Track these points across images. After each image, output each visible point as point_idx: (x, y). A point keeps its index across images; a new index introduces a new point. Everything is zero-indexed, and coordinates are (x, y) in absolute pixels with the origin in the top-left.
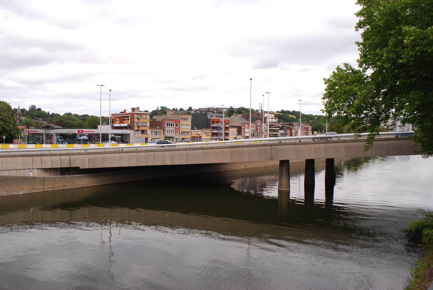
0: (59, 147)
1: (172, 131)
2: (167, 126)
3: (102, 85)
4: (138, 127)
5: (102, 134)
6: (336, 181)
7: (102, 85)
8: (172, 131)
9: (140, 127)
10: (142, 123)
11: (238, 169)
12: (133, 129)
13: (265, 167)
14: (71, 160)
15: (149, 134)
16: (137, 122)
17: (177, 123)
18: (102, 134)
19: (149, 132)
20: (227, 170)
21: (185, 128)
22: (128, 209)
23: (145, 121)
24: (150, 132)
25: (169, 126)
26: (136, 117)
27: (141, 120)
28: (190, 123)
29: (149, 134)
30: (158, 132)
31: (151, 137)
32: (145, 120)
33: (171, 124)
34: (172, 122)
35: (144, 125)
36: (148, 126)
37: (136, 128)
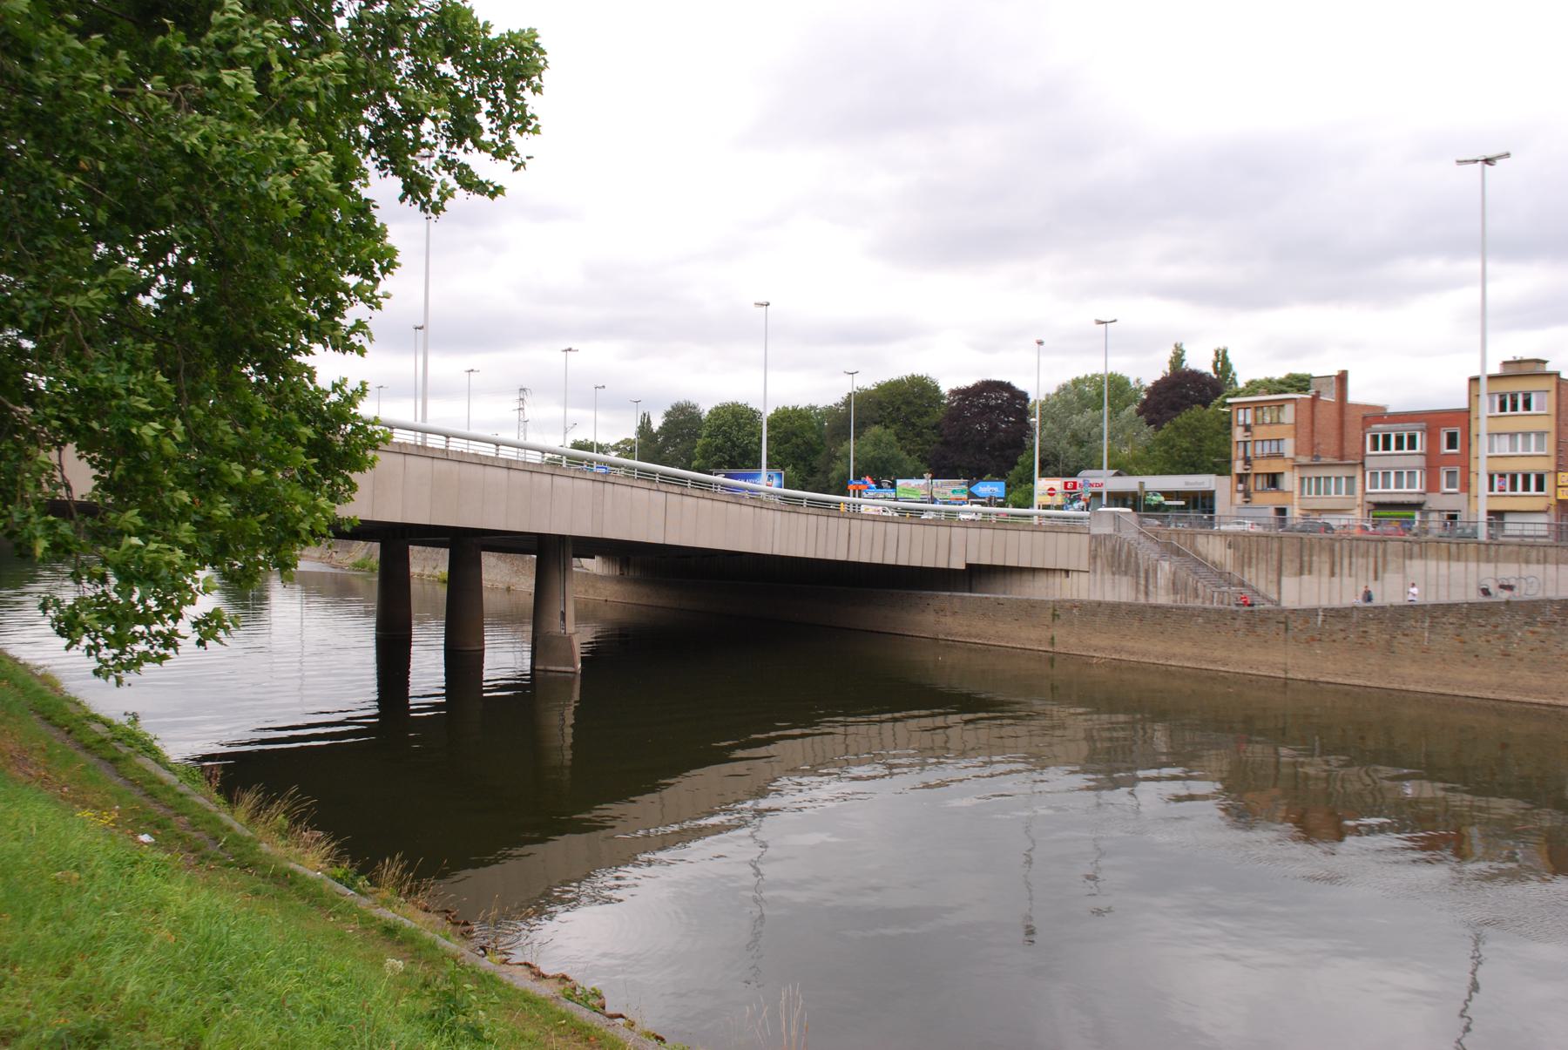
0: (1354, 560)
1: (1399, 474)
2: (1375, 448)
3: (570, 350)
4: (1247, 461)
5: (1108, 493)
6: (443, 691)
7: (570, 350)
8: (1386, 475)
9: (1255, 463)
10: (1259, 445)
11: (1003, 644)
12: (1095, 462)
13: (1116, 666)
14: (1027, 577)
15: (1292, 492)
16: (1245, 442)
17: (1452, 430)
18: (1108, 493)
19: (1290, 481)
20: (943, 637)
21: (1533, 452)
22: (1079, 780)
23: (1275, 432)
24: (1297, 481)
25: (1386, 447)
26: (1241, 418)
27: (1260, 432)
28: (1549, 425)
29: (1292, 492)
30: (1329, 478)
31: (1300, 505)
32: (1273, 427)
33: (1399, 440)
34: (1405, 430)
35: (1274, 451)
36: (1286, 456)
37: (1238, 467)
